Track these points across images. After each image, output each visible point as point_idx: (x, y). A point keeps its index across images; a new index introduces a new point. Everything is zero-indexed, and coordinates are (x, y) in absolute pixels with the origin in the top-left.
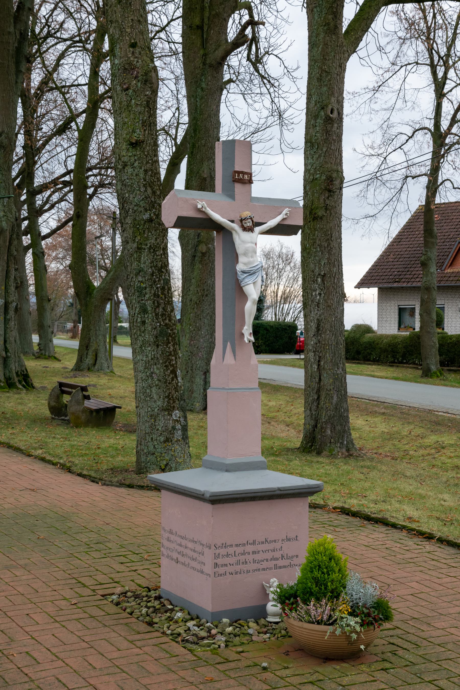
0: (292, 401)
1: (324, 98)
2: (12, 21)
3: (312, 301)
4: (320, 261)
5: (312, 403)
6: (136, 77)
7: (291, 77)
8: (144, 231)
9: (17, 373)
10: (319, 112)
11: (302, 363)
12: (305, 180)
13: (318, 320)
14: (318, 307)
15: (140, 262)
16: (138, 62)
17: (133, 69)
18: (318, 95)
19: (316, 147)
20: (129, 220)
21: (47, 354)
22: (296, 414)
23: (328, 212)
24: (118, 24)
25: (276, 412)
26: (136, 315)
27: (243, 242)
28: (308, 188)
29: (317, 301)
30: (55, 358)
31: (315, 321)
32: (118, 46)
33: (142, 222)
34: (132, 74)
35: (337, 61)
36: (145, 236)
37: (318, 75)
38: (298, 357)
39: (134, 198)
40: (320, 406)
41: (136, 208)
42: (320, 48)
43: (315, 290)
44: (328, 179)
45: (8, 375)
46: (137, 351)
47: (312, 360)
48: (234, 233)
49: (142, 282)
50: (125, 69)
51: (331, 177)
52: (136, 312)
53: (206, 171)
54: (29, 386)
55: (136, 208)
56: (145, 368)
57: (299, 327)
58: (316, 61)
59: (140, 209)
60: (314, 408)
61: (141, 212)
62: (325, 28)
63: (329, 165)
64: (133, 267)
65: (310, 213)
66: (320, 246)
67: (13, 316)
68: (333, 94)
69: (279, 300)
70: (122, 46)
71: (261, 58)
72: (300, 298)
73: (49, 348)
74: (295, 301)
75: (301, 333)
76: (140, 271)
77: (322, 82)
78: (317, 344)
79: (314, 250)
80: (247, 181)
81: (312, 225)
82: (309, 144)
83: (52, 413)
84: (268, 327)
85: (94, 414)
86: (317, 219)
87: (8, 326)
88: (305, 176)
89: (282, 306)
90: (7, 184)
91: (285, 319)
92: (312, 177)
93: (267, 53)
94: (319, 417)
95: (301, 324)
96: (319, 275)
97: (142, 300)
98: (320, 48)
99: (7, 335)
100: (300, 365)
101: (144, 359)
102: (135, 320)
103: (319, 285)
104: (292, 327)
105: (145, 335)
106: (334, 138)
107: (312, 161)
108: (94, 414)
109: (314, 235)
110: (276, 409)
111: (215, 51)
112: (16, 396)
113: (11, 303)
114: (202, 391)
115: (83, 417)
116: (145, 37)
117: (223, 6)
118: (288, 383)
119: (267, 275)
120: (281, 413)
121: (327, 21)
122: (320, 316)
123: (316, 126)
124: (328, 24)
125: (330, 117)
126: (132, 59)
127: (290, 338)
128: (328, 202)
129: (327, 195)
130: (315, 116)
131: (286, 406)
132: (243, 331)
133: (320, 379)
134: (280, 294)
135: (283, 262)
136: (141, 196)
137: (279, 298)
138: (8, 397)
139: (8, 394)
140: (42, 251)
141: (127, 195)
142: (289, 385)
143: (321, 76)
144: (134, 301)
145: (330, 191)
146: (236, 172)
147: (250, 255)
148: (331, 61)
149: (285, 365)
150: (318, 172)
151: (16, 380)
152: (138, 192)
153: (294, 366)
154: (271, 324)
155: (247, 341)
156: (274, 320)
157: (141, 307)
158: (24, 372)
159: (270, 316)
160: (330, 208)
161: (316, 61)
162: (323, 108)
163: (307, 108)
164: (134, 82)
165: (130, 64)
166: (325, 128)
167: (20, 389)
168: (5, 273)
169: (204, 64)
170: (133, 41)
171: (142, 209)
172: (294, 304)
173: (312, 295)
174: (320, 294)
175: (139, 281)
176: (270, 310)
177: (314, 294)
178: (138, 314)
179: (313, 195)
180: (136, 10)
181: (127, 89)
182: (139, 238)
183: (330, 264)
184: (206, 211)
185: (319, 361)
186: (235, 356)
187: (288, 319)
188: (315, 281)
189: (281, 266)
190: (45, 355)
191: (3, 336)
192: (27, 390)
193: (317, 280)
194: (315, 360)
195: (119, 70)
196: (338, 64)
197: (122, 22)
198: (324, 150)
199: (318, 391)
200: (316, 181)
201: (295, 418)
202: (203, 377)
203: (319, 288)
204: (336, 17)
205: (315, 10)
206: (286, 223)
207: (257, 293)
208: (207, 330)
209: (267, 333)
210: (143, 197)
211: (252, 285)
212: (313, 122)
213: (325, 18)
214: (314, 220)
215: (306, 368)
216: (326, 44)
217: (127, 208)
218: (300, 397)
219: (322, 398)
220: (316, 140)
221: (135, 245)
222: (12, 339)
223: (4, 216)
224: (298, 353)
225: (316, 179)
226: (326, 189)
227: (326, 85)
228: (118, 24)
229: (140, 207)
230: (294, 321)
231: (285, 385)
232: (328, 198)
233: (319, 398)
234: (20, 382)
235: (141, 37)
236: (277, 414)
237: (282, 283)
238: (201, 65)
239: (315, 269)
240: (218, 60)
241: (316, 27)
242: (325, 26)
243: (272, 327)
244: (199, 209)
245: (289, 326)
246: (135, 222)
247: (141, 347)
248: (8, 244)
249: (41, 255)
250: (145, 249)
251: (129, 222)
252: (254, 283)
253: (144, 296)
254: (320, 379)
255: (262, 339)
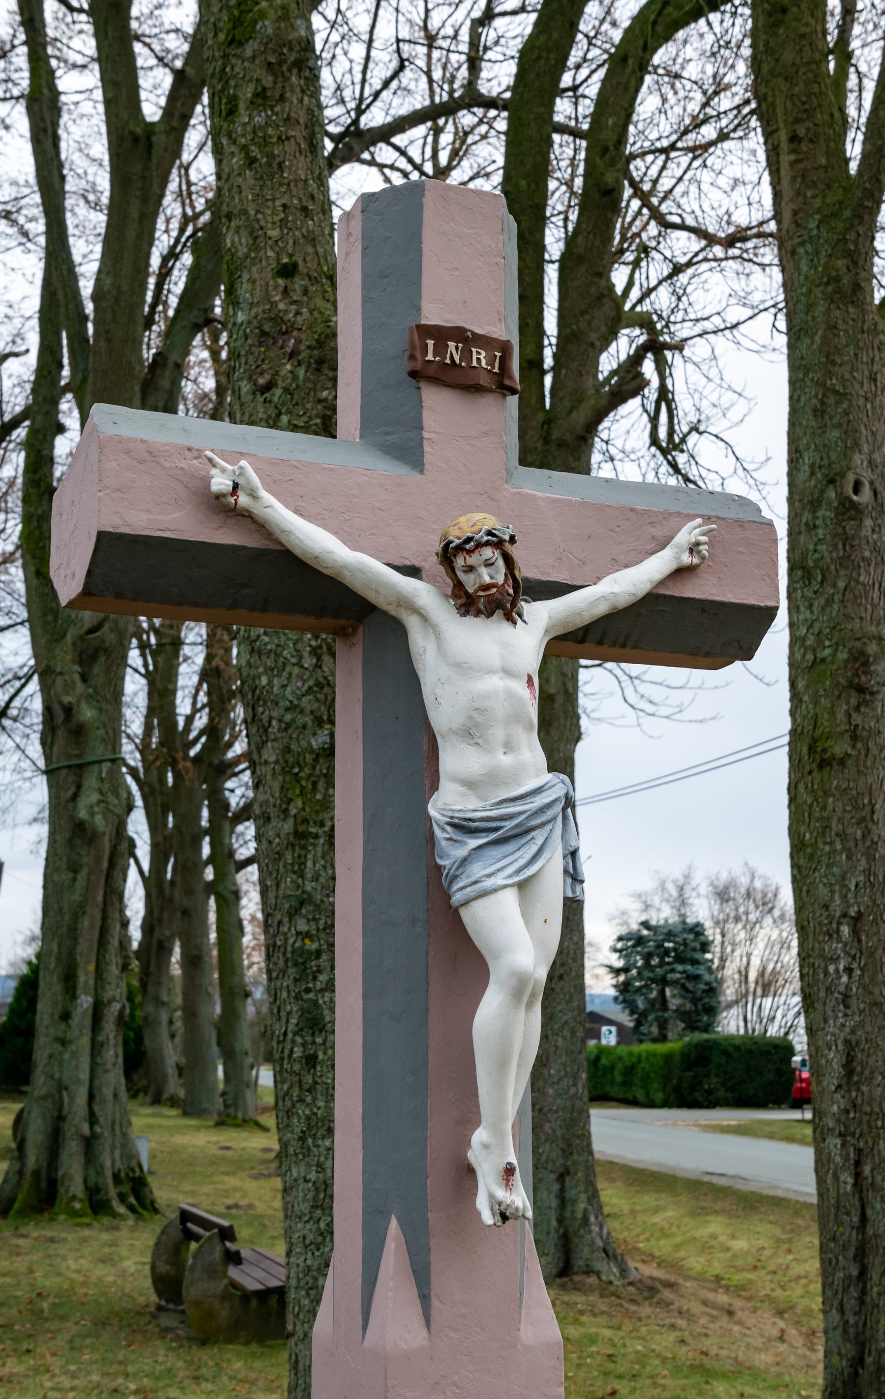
0: (790, 1241)
1: (834, 457)
2: (137, 389)
3: (828, 989)
4: (843, 878)
5: (846, 1289)
6: (292, 355)
7: (752, 482)
8: (314, 784)
9: (116, 1177)
10: (822, 491)
11: (808, 1131)
12: (793, 664)
13: (847, 1042)
14: (847, 1007)
15: (302, 876)
16: (298, 313)
17: (287, 332)
18: (816, 449)
19: (819, 578)
20: (270, 754)
21: (240, 1115)
22: (799, 1278)
23: (859, 745)
24: (247, 220)
25: (749, 1271)
26: (290, 1036)
27: (463, 668)
28: (801, 684)
29: (842, 989)
30: (257, 1124)
31: (840, 1047)
32: (246, 276)
33: (309, 758)
34: (282, 347)
35: (865, 367)
36: (319, 797)
37: (815, 401)
38: (796, 1115)
39: (284, 687)
40: (868, 1299)
41: (288, 717)
42: (817, 339)
43: (835, 960)
44: (856, 659)
45: (93, 1179)
46: (291, 1150)
47: (838, 1159)
48: (413, 624)
49: (307, 935)
50: (264, 334)
51: (862, 653)
52: (291, 1027)
53: (553, 680)
54: (144, 1207)
55: (288, 717)
56: (314, 1207)
57: (798, 1048)
58: (807, 369)
59: (301, 720)
60: (851, 1303)
61: (304, 727)
62: (830, 289)
63: (857, 624)
64: (281, 892)
65: (811, 749)
66: (842, 836)
67: (111, 1036)
68: (856, 445)
69: (751, 990)
70: (256, 276)
71: (683, 440)
72: (797, 985)
73: (244, 1101)
74: (785, 991)
75: (803, 1063)
76: (302, 903)
77: (826, 417)
78: (847, 1112)
79: (827, 848)
80: (484, 380)
81: (817, 781)
82: (799, 573)
83: (160, 1293)
84: (730, 1049)
85: (254, 1303)
86: (830, 764)
87: (99, 1060)
88: (792, 656)
89: (758, 1001)
90: (111, 732)
91: (766, 1031)
92: (810, 657)
93: (695, 429)
94: (868, 1333)
95: (800, 1041)
96: (845, 915)
97: (308, 990)
98: (817, 339)
99: (97, 1083)
100: (805, 1136)
101: (313, 1176)
102: (287, 1052)
103: (846, 944)
104: (784, 1048)
105: (314, 1099)
106: (867, 554)
107: (808, 614)
108: (254, 1303)
109: (824, 808)
110: (751, 1261)
111: (570, 412)
112: (105, 1237)
113: (109, 1003)
114: (554, 1223)
115: (224, 1313)
116: (320, 250)
117: (587, 317)
118: (776, 1187)
119: (723, 936)
120: (763, 1273)
121: (834, 274)
122: (853, 1032)
123: (815, 527)
124: (837, 279)
125: (851, 501)
126: (282, 306)
127: (779, 1072)
128: (857, 719)
129: (854, 701)
130: (811, 503)
131: (775, 1254)
132: (475, 1155)
133: (864, 1218)
134: (753, 975)
135: (757, 907)
136: (305, 681)
137: (752, 986)
138: (84, 1241)
139: (86, 1232)
140: (234, 888)
141: (264, 680)
142: (779, 1193)
143: (822, 403)
144: (285, 995)
145: (861, 690)
146: (426, 331)
147: (498, 734)
148: (847, 368)
149: (771, 1136)
150: (827, 643)
151: (113, 1192)
152: (296, 670)
153: (790, 1139)
154: (737, 1042)
155: (488, 1218)
156: (742, 1032)
157: (303, 1011)
158: (133, 1170)
159: (733, 1023)
160: (865, 734)
161: (807, 369)
162: (832, 481)
163: (791, 485)
164: (288, 367)
165: (277, 319)
166: (840, 530)
167: (120, 1215)
168: (97, 932)
169: (546, 441)
170: (286, 260)
171: (308, 720)
172: (783, 998)
173: (826, 972)
174: (849, 970)
175: (298, 933)
176: (734, 1011)
177: (831, 968)
178: (295, 1034)
179: (816, 703)
180: (296, 180)
181: (269, 387)
182: (299, 803)
183: (872, 885)
184: (257, 509)
185: (858, 1163)
186: (425, 1299)
187: (773, 1031)
188: (833, 934)
189: (752, 917)
190: (235, 1118)
191: (87, 1084)
192: (139, 1217)
193: (838, 931)
194: (846, 1159)
195: (246, 337)
196: (866, 373)
197: (258, 212)
198: (841, 584)
199: (861, 1254)
200: (822, 667)
201: (799, 1291)
202: (556, 1187)
203: (847, 953)
204: (855, 263)
205: (801, 250)
206: (692, 590)
207: (538, 942)
208: (564, 1065)
209: (727, 1062)
210: (311, 683)
211: (509, 899)
212: (806, 516)
213: (826, 266)
214: (821, 767)
215: (819, 1141)
216: (832, 328)
217: (265, 718)
218: (807, 1227)
219: (875, 1275)
220: (817, 561)
221: (288, 826)
222: (108, 1092)
223: (100, 802)
224: (797, 1105)
225: (823, 660)
226: (850, 685)
227: (839, 426)
228: (247, 220)
229: (302, 712)
230: (787, 1034)
231: (770, 1192)
232: (857, 709)
233: (863, 1273)
234: (122, 1198)
235: (310, 250)
236: (752, 1276)
237: (756, 952)
238: (539, 445)
239: (832, 899)
240: (579, 430)
241: (804, 290)
242: (827, 284)
243: (737, 1048)
244: (218, 496)
245: (776, 1047)
246: (287, 757)
247: (302, 1139)
248: (105, 865)
249: (232, 897)
250: (316, 836)
251: (272, 759)
252: (522, 886)
253: (315, 978)
254: (864, 1218)
255: (717, 1076)
